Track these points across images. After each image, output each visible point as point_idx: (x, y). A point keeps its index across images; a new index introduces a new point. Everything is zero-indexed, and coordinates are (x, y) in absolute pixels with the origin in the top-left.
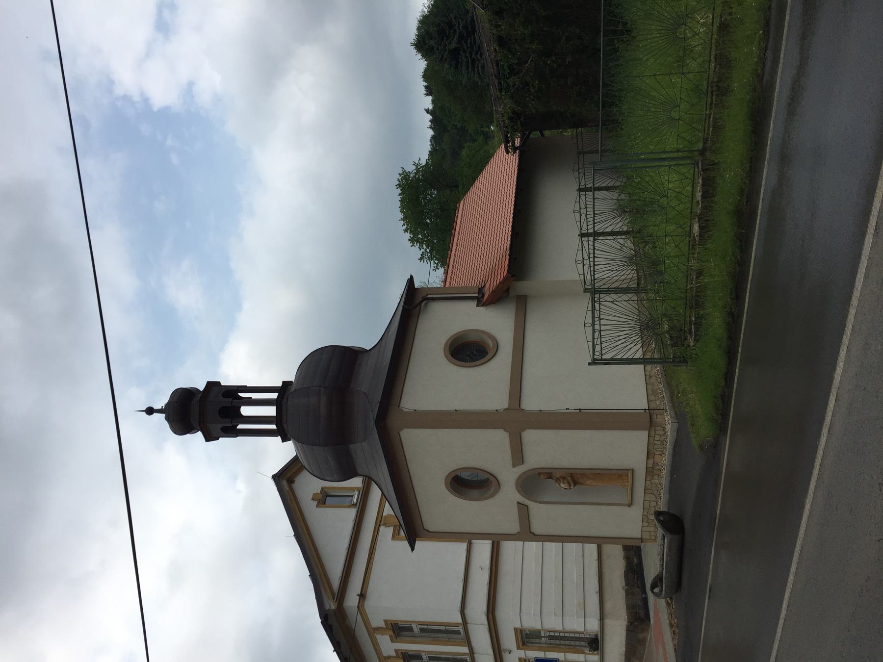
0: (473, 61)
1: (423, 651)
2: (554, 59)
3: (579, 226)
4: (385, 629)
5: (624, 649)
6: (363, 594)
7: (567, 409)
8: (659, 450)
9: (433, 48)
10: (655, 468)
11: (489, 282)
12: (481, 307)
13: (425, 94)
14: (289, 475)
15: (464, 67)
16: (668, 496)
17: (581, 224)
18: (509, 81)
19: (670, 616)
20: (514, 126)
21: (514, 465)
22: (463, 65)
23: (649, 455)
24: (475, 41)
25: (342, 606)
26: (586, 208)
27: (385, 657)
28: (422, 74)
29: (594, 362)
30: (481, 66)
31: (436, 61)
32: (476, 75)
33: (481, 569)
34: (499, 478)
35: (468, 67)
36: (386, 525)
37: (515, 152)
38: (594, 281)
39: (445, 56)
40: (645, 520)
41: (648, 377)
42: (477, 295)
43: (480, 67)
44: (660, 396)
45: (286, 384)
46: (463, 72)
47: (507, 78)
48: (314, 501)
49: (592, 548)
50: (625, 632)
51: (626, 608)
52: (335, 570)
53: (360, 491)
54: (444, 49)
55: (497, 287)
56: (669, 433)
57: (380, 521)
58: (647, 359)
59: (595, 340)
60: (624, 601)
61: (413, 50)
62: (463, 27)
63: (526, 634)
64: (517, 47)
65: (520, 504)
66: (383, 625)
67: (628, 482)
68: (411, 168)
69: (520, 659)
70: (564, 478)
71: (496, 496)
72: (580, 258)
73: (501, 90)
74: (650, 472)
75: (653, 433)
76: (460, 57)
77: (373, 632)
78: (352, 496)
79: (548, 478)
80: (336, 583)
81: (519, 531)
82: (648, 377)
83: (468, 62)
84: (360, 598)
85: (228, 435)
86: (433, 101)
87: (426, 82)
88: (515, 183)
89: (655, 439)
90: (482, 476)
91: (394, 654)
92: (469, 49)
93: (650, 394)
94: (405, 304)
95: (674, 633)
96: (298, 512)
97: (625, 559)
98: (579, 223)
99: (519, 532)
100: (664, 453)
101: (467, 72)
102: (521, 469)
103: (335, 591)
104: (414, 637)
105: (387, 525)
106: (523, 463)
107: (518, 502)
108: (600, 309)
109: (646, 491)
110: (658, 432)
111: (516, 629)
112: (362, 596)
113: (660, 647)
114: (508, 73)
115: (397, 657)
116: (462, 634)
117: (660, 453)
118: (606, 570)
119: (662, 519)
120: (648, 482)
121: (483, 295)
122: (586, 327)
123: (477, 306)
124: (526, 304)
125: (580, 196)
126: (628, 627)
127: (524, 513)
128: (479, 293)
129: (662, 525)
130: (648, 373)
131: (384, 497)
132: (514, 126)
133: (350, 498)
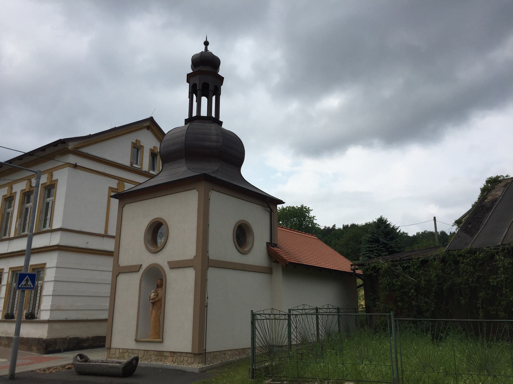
0: (372, 251)
1: (13, 209)
2: (414, 294)
3: (321, 308)
4: (51, 180)
5: (25, 337)
6: (76, 167)
7: (208, 297)
8: (177, 360)
9: (380, 228)
10: (163, 357)
11: (281, 250)
12: (266, 246)
13: (344, 225)
14: (152, 126)
15: (369, 246)
16: (144, 366)
17: (322, 309)
18: (399, 266)
19: (56, 367)
20: (370, 269)
21: (169, 263)
22: (370, 245)
23: (173, 353)
24: (383, 252)
25: (70, 153)
26: (275, 319)
27: (12, 186)
28: (355, 224)
29: (253, 315)
30: (370, 255)
31: (372, 230)
32: (365, 252)
33: (87, 243)
34: (160, 253)
35: (369, 248)
36: (118, 184)
37: (352, 270)
38: (321, 315)
39: (375, 235)
40: (124, 351)
41: (224, 352)
42: (273, 243)
43: (369, 255)
44: (213, 360)
45: (221, 123)
46: (367, 245)
47: (401, 265)
48: (136, 141)
49: (105, 315)
50: (38, 338)
51: (55, 338)
52: (93, 150)
53: (140, 169)
54: (379, 234)
55: (280, 255)
56: (190, 366)
57: (121, 180)
58: (291, 346)
59: (264, 316)
60: (59, 337)
61: (378, 217)
62: (391, 246)
63: (40, 271)
64: (421, 271)
65: (140, 267)
66: (54, 178)
67: (153, 339)
68: (312, 214)
69: (3, 269)
70: (157, 295)
71: (147, 252)
72: (306, 307)
73: (392, 261)
74: (160, 354)
75: (190, 356)
76: (375, 244)
77: (50, 172)
78: (137, 164)
79: (157, 285)
80: (85, 150)
81: (120, 266)
82: (244, 350)
83: (372, 248)
84: (73, 164)
85: (191, 88)
86: (339, 229)
87: (350, 225)
88: (334, 269)
89: (184, 358)
90: (160, 241)
91: (54, 178)
92: (379, 249)
93: (216, 354)
94: (272, 198)
95: (44, 370)
96: (131, 130)
97: (87, 338)
98: (322, 307)
99: (119, 266)
100: (174, 363)
101: (366, 247)
102: (166, 268)
103: (79, 149)
104: (44, 198)
105: (118, 184)
106: (170, 268)
107: (141, 265)
108: (280, 319)
109: (146, 352)
110: (190, 359)
111: (45, 264)
112: (75, 166)
113: (29, 361)
114: (404, 266)
115: (52, 181)
116: (44, 229)
117: (174, 361)
118: (80, 324)
119: (134, 362)
120: (152, 353)
121: (273, 247)
122: (271, 309)
123: (267, 242)
124: (268, 273)
125: (313, 309)
126: (42, 339)
127: (133, 269)
128: (274, 244)
129: (130, 361)
130: (226, 352)
131: (139, 184)
132: (370, 269)
133: (135, 163)
